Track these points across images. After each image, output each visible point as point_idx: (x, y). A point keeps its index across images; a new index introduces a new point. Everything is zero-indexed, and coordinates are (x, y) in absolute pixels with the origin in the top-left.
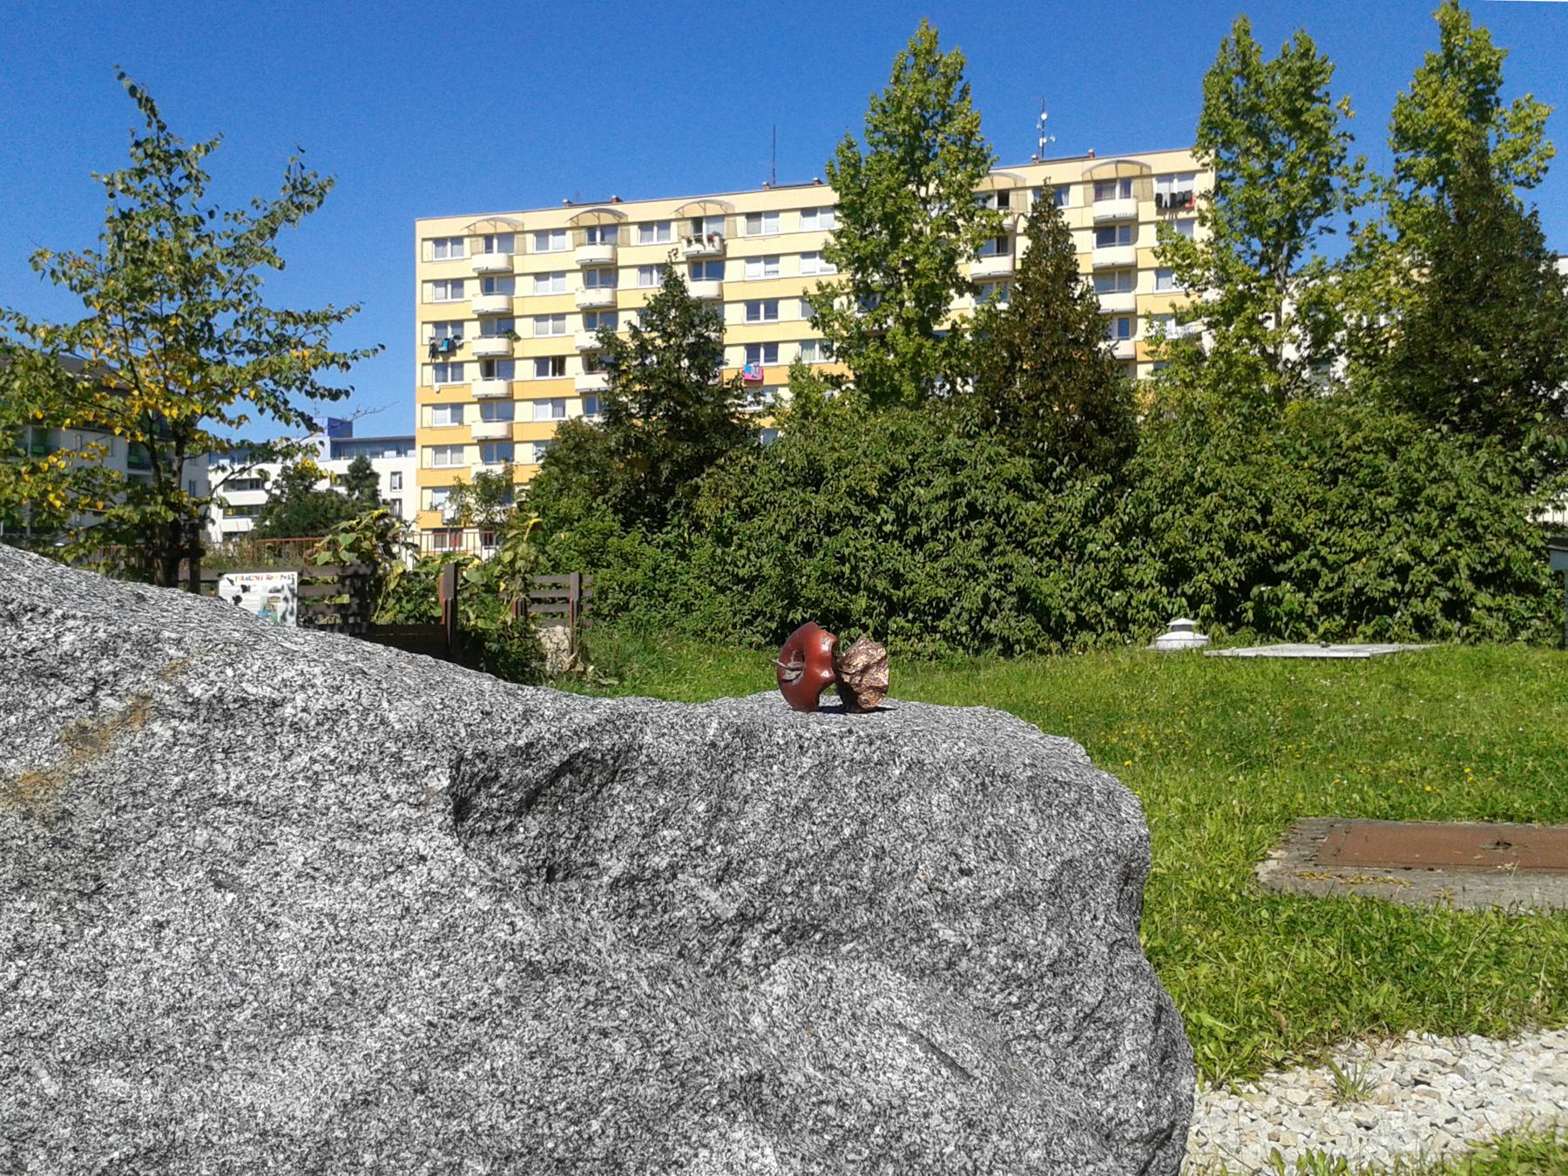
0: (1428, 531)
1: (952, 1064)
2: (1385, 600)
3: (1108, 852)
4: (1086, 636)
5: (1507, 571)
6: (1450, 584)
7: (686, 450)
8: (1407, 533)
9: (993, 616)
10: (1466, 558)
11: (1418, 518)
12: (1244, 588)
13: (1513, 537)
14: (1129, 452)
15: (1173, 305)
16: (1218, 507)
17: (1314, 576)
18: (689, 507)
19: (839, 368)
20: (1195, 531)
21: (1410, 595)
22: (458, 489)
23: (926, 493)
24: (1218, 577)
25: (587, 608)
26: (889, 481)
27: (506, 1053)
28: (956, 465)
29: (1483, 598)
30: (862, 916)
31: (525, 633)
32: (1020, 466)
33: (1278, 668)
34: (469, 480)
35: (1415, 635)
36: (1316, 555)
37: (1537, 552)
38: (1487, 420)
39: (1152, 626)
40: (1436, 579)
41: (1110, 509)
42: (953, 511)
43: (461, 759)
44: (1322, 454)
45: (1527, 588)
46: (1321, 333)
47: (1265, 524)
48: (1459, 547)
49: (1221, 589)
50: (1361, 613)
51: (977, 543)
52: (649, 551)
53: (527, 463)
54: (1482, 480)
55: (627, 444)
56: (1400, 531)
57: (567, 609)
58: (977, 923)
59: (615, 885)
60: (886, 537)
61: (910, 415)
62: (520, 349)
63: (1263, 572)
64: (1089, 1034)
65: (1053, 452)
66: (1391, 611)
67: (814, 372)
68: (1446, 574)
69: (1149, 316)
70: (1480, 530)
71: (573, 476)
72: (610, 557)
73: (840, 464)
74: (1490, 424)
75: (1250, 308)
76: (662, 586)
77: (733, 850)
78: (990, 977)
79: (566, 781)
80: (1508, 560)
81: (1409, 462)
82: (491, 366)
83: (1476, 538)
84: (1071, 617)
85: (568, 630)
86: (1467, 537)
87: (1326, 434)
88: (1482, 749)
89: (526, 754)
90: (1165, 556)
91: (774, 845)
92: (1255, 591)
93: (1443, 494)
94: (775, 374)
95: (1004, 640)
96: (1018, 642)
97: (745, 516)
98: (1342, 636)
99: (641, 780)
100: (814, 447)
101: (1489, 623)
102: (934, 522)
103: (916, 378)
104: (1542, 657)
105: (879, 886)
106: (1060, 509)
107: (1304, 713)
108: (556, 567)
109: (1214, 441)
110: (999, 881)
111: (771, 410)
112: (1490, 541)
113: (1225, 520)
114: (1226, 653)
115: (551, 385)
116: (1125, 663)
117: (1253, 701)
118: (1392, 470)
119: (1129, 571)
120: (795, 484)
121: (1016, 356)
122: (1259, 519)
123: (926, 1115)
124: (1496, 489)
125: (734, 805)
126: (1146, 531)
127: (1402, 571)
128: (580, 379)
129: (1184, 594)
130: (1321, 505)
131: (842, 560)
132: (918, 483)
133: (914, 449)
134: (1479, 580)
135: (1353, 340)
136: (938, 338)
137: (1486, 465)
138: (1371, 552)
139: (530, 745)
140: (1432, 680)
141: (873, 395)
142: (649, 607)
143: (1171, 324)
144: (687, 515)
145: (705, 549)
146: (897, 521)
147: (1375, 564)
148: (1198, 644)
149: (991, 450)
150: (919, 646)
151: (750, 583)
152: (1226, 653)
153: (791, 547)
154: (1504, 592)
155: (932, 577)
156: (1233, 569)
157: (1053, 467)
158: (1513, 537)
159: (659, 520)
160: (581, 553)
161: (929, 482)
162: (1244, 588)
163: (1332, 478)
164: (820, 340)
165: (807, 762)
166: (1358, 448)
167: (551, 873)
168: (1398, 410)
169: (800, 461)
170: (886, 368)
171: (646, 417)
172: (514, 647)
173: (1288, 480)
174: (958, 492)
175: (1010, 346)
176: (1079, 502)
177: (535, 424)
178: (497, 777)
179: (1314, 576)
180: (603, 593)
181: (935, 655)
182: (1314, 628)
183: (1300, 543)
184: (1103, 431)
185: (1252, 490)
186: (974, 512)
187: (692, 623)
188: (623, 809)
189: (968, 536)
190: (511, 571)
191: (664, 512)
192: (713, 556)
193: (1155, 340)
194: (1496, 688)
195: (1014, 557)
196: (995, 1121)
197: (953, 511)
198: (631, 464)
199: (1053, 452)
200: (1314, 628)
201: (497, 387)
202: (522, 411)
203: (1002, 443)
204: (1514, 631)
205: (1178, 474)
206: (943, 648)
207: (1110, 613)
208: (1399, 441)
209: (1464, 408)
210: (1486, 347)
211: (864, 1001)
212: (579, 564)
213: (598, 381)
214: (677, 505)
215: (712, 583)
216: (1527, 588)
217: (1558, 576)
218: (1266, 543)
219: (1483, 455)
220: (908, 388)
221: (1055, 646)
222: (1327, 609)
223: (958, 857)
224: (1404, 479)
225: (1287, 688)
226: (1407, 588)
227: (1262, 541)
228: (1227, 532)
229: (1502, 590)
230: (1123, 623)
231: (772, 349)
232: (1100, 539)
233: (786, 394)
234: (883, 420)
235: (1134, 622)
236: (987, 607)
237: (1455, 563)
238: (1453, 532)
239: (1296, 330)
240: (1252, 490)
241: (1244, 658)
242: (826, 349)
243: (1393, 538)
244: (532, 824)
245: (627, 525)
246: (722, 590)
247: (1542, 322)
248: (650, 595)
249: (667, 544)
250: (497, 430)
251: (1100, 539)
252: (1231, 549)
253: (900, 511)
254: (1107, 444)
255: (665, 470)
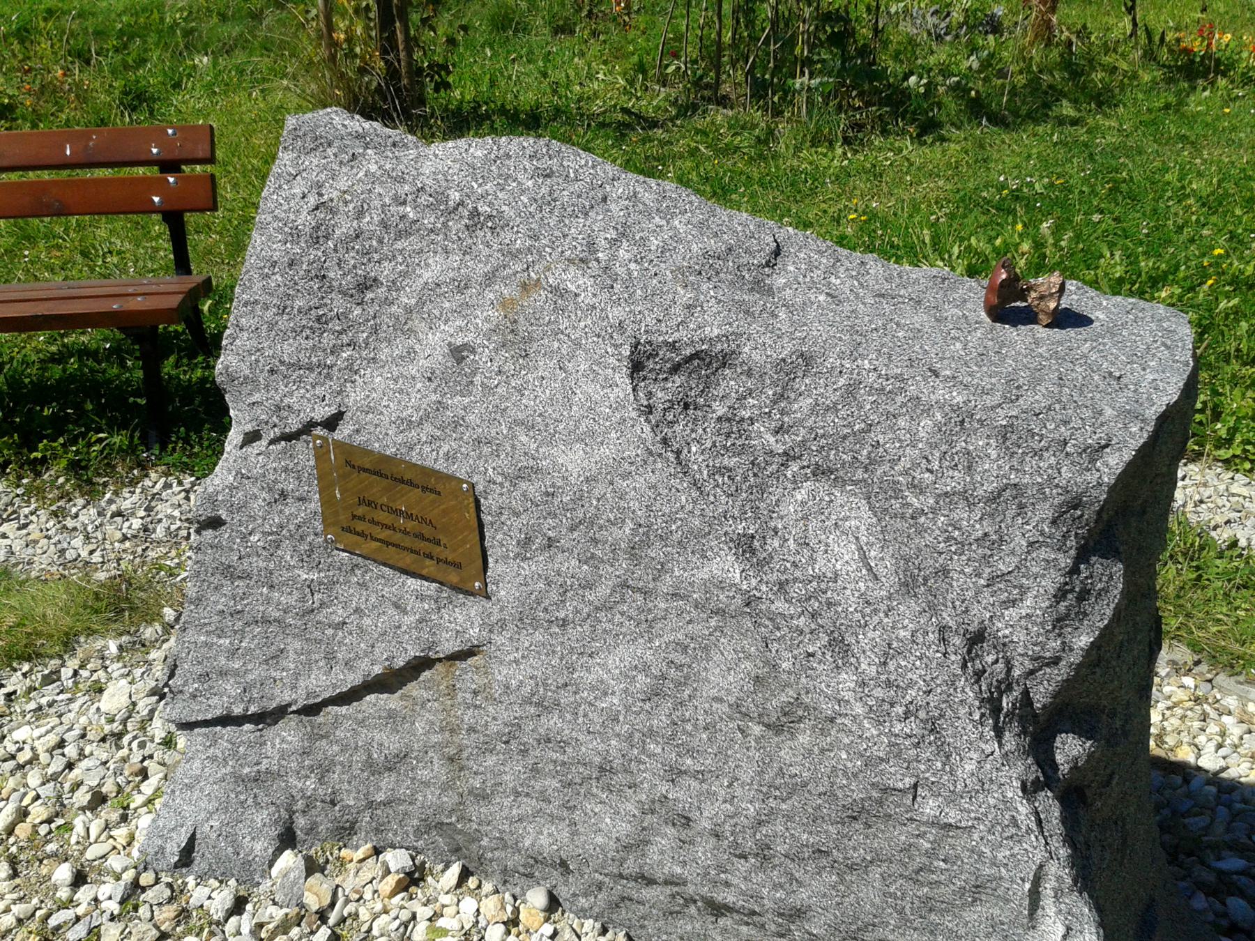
1: (870, 569)
3: (1057, 486)
27: (640, 482)
30: (860, 474)
43: (639, 343)
58: (932, 501)
59: (719, 419)
64: (1001, 586)
77: (786, 419)
78: (937, 532)
79: (696, 363)
89: (673, 346)
91: (809, 423)
99: (739, 370)
105: (872, 462)
110: (953, 481)
123: (845, 588)
125: (792, 396)
139: (675, 342)
165: (842, 382)
167: (686, 407)
178: (657, 354)
188: (730, 383)
196: (883, 607)
211: (846, 519)
223: (928, 460)
244: (678, 380)
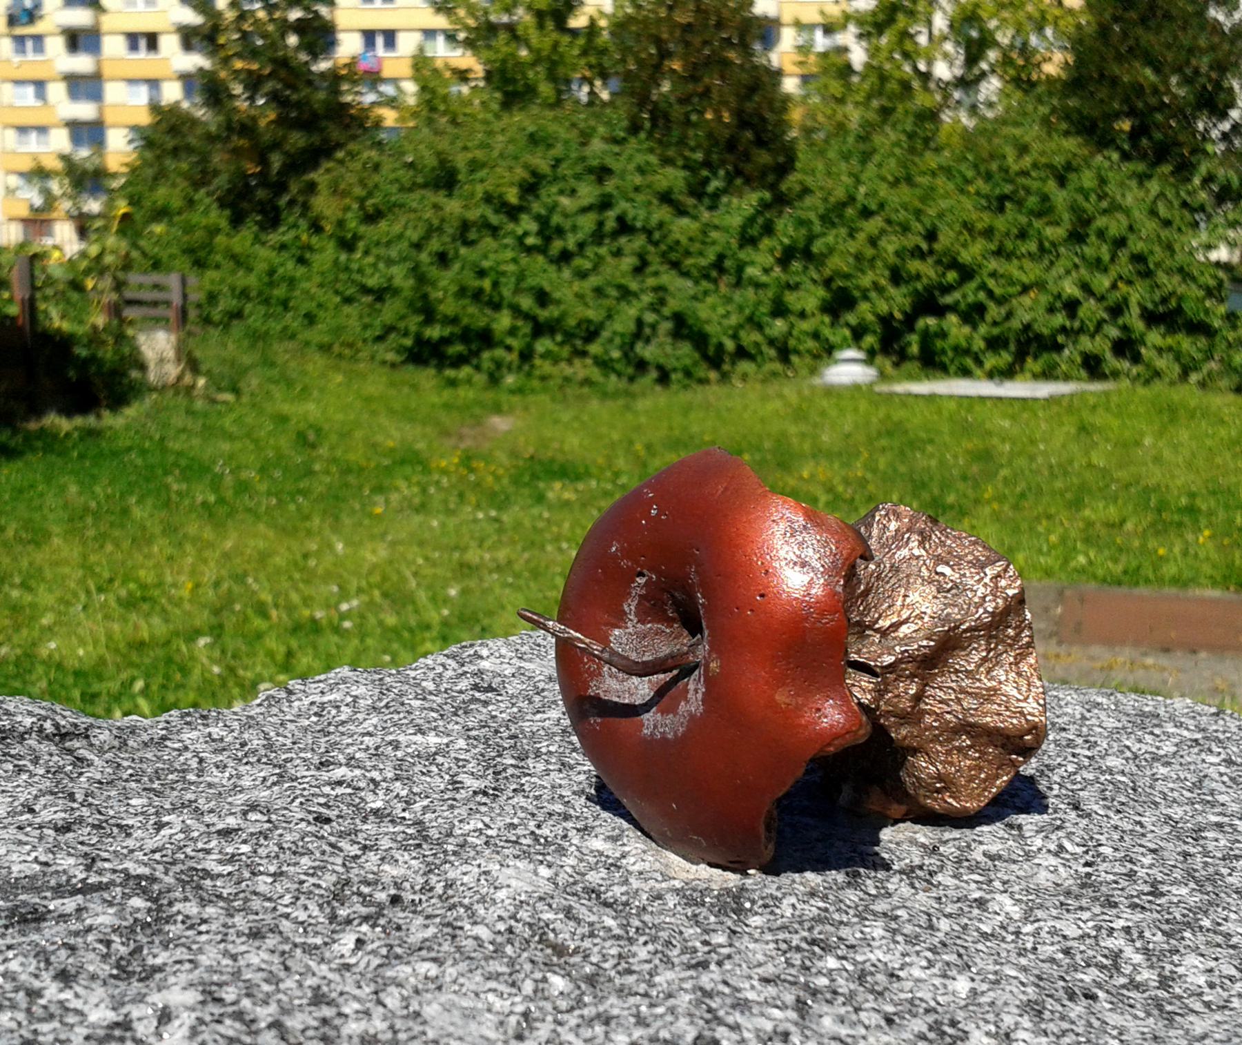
0: (1098, 265)
2: (1053, 337)
4: (745, 366)
5: (1179, 310)
6: (1120, 322)
7: (297, 140)
8: (1076, 266)
9: (648, 341)
10: (1137, 295)
11: (1088, 251)
12: (910, 321)
13: (1185, 274)
14: (785, 168)
15: (822, 13)
16: (883, 232)
17: (980, 309)
18: (306, 207)
19: (463, 58)
20: (858, 257)
21: (1081, 330)
22: (39, 174)
23: (572, 202)
24: (883, 307)
25: (193, 314)
26: (530, 188)
28: (602, 173)
29: (1155, 337)
31: (120, 338)
32: (673, 178)
33: (952, 405)
34: (54, 164)
35: (1083, 373)
36: (983, 286)
37: (1209, 292)
38: (1162, 146)
39: (816, 357)
40: (1105, 316)
41: (768, 229)
42: (601, 224)
44: (988, 177)
45: (1198, 328)
46: (974, 51)
47: (931, 252)
48: (1130, 283)
49: (886, 320)
50: (1027, 349)
51: (628, 262)
52: (264, 252)
53: (119, 148)
54: (1153, 213)
55: (229, 127)
56: (1069, 264)
57: (171, 314)
60: (529, 250)
61: (550, 114)
62: (107, 22)
63: (928, 303)
65: (707, 164)
66: (1059, 348)
67: (439, 64)
68: (1117, 311)
69: (798, 25)
70: (1151, 266)
71: (170, 163)
72: (218, 258)
73: (474, 166)
74: (1161, 154)
75: (901, 19)
76: (279, 292)
80: (1180, 299)
81: (1081, 190)
82: (76, 40)
83: (1147, 274)
84: (730, 345)
85: (173, 338)
86: (1139, 273)
87: (992, 157)
88: (1184, 501)
90: (827, 283)
92: (921, 323)
93: (1116, 225)
94: (395, 63)
95: (660, 368)
96: (675, 370)
97: (372, 218)
98: (1007, 373)
100: (443, 144)
101: (1161, 363)
102: (580, 236)
103: (552, 77)
104: (1223, 401)
106: (716, 228)
107: (985, 456)
108: (156, 265)
109: (877, 158)
111: (391, 102)
112: (1162, 277)
113: (890, 246)
114: (900, 388)
115: (142, 61)
116: (793, 398)
117: (931, 441)
118: (1060, 197)
119: (790, 298)
120: (425, 186)
121: (664, 54)
122: (924, 246)
124: (1167, 223)
126: (808, 255)
127: (1071, 307)
128: (179, 59)
129: (848, 325)
130: (988, 233)
131: (482, 273)
132: (561, 192)
133: (558, 151)
134: (1151, 318)
135: (1006, 61)
136: (574, 33)
137: (1157, 197)
138: (1040, 285)
140: (1115, 423)
141: (506, 94)
142: (267, 316)
143: (819, 35)
144: (303, 215)
145: (326, 254)
146: (540, 233)
147: (1044, 299)
148: (867, 379)
149: (640, 159)
150: (569, 371)
151: (380, 294)
152: (900, 388)
153: (424, 257)
154: (1175, 332)
155: (580, 296)
156: (897, 301)
157: (706, 181)
158: (1185, 274)
159: (272, 219)
160: (185, 252)
161: (573, 192)
162: (910, 321)
163: (999, 202)
164: (444, 31)
166: (1024, 173)
168: (1067, 134)
169: (430, 161)
170: (519, 64)
171: (252, 99)
172: (107, 353)
173: (956, 205)
174: (605, 204)
175: (658, 42)
176: (736, 221)
177: (126, 105)
179: (980, 309)
180: (212, 298)
181: (587, 382)
182: (979, 363)
183: (967, 273)
184: (760, 142)
185: (918, 213)
186: (624, 227)
187: (318, 334)
189: (618, 253)
190: (97, 266)
191: (276, 209)
192: (336, 262)
193: (804, 49)
194: (1184, 435)
195: (669, 278)
197: (601, 224)
198: (236, 151)
199: (707, 164)
200: (979, 363)
201: (82, 63)
202: (114, 92)
203: (651, 150)
204: (1185, 374)
205: (840, 194)
206: (595, 373)
207: (771, 342)
208: (1069, 167)
209: (1134, 135)
210: (1157, 70)
212: (183, 263)
213: (196, 61)
214: (292, 203)
215: (337, 292)
216: (1198, 328)
217: (1231, 317)
218: (932, 273)
219: (1154, 187)
220: (545, 89)
221: (713, 375)
222: (995, 344)
224: (1074, 209)
225: (965, 429)
226: (1077, 324)
227: (927, 270)
228: (892, 259)
229: (1172, 329)
230: (784, 354)
231: (390, 37)
232: (759, 262)
233: (410, 87)
234: (518, 119)
235: (797, 352)
236: (640, 332)
237: (1126, 300)
238: (1124, 266)
239: (949, 47)
240: (918, 213)
241: (917, 396)
242: (451, 37)
243: (1062, 271)
245: (237, 221)
246: (348, 300)
247: (1213, 48)
248: (267, 302)
249: (283, 247)
250: (85, 111)
251: (759, 262)
252: (897, 277)
253: (543, 221)
254: (764, 158)
255: (276, 161)
